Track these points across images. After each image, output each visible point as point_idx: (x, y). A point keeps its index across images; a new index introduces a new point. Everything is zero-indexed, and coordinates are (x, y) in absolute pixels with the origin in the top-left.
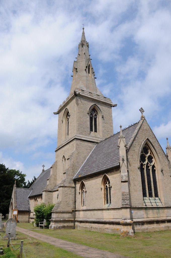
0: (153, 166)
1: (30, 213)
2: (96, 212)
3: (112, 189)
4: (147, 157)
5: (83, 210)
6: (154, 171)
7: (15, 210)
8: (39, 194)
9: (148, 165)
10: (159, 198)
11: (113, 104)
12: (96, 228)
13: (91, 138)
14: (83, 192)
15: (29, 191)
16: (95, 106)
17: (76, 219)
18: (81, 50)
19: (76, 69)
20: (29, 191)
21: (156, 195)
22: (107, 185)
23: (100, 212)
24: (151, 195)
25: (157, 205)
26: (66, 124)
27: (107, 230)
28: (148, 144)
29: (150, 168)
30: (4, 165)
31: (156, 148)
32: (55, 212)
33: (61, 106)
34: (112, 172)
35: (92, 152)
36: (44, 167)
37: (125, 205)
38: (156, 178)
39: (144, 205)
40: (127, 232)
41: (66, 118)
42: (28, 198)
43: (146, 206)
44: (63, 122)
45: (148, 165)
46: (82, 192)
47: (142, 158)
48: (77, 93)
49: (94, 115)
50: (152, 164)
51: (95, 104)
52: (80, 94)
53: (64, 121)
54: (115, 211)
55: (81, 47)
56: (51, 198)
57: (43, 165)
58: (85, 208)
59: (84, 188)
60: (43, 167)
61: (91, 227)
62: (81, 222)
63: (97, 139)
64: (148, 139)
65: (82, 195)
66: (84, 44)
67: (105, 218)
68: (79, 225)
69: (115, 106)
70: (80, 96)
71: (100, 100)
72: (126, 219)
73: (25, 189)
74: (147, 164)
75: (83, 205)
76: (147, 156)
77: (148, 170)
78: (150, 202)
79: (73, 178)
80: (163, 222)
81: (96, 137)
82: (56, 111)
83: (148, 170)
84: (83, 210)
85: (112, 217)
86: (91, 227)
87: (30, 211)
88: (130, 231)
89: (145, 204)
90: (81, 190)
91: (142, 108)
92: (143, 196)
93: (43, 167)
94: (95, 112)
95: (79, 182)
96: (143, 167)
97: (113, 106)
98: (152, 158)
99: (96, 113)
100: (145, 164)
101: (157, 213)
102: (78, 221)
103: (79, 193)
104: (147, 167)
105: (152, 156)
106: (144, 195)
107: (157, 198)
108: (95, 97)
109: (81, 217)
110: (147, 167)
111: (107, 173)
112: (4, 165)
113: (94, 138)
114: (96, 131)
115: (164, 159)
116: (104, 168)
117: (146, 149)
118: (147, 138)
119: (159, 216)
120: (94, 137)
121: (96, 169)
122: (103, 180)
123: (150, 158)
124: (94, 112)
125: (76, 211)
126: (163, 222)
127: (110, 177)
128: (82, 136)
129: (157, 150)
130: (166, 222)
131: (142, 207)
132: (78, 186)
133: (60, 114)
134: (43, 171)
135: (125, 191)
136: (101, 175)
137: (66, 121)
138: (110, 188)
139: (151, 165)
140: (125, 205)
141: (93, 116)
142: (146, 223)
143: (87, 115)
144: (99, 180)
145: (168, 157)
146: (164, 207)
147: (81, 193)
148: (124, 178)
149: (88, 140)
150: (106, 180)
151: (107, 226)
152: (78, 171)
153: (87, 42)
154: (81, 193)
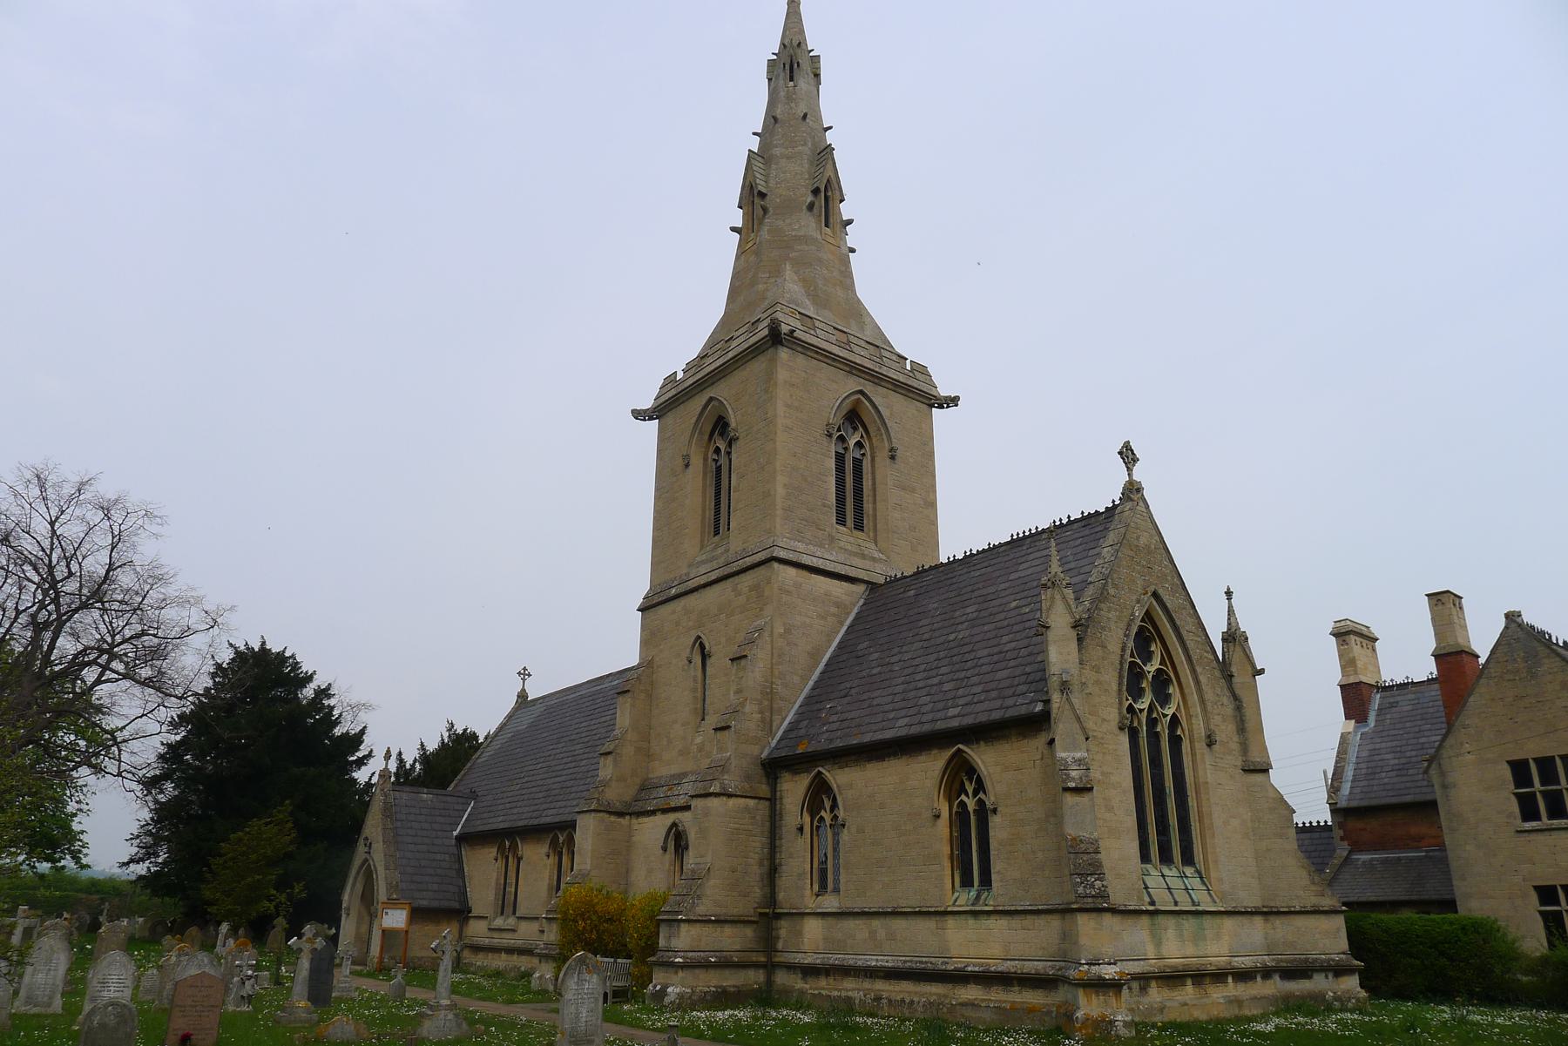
0: (1175, 721)
1: (467, 919)
2: (899, 924)
3: (995, 821)
4: (1150, 676)
5: (824, 915)
6: (1176, 742)
7: (392, 903)
8: (536, 822)
9: (1154, 715)
10: (1199, 872)
11: (944, 391)
12: (903, 1001)
13: (841, 558)
14: (818, 827)
15: (460, 807)
16: (858, 401)
17: (779, 958)
18: (782, 94)
19: (762, 195)
20: (460, 807)
21: (1188, 859)
22: (963, 797)
23: (926, 926)
24: (1166, 858)
25: (1194, 903)
26: (704, 478)
27: (969, 1012)
28: (1153, 614)
29: (1163, 728)
30: (293, 656)
31: (1184, 633)
32: (681, 920)
33: (671, 379)
34: (998, 738)
35: (845, 628)
36: (528, 680)
37: (1093, 896)
38: (1183, 774)
39: (1147, 899)
40: (1104, 1020)
41: (707, 447)
42: (454, 842)
43: (1152, 903)
44: (687, 466)
45: (1154, 715)
46: (815, 823)
47: (1133, 681)
48: (785, 329)
49: (852, 442)
50: (1169, 711)
51: (861, 392)
52: (798, 334)
53: (697, 462)
54: (1016, 922)
55: (783, 76)
56: (620, 854)
57: (520, 669)
58: (830, 903)
59: (827, 804)
60: (524, 680)
61: (878, 999)
62: (810, 971)
63: (867, 564)
64: (1155, 595)
65: (815, 838)
66: (798, 66)
67: (954, 952)
68: (798, 986)
69: (953, 401)
70: (794, 347)
71: (884, 371)
72: (1099, 964)
73: (435, 791)
74: (1151, 708)
75: (816, 887)
76: (1149, 672)
77: (1154, 737)
78: (1166, 883)
79: (764, 756)
80: (1219, 976)
81: (863, 556)
82: (647, 403)
83: (1154, 737)
84: (824, 915)
85: (997, 951)
86: (878, 999)
87: (470, 912)
88: (1120, 1018)
89: (1149, 895)
90: (807, 818)
91: (1128, 442)
92: (1143, 862)
93: (524, 680)
94: (855, 429)
95: (796, 773)
96: (1179, 733)
97: (941, 407)
98: (1168, 681)
99: (862, 437)
100: (1141, 711)
101: (1198, 938)
102: (791, 967)
103: (801, 829)
104: (1152, 722)
105: (1167, 674)
106: (1145, 857)
107: (1189, 871)
108: (860, 357)
109: (806, 948)
110: (1152, 722)
111: (967, 742)
112: (293, 656)
113: (857, 562)
114: (859, 526)
115: (1218, 691)
116: (954, 718)
117: (1145, 637)
118: (1152, 588)
119: (1201, 953)
120: (856, 554)
121: (906, 721)
122: (946, 769)
123: (1161, 683)
124: (850, 430)
125: (778, 916)
126: (1219, 976)
127: (986, 758)
128: (801, 546)
129: (1190, 645)
130: (1230, 979)
131: (1137, 908)
132: (794, 789)
133: (670, 418)
134: (522, 695)
135: (1081, 834)
136: (935, 752)
137: (705, 459)
138: (983, 812)
139: (1166, 716)
140: (1090, 900)
141: (846, 449)
142: (1208, 980)
143: (825, 439)
144: (928, 769)
145: (1234, 680)
146: (1222, 909)
147: (807, 829)
148: (1074, 774)
149: (830, 567)
150: (961, 776)
151: (971, 993)
152: (784, 719)
153: (811, 54)
154: (807, 829)
